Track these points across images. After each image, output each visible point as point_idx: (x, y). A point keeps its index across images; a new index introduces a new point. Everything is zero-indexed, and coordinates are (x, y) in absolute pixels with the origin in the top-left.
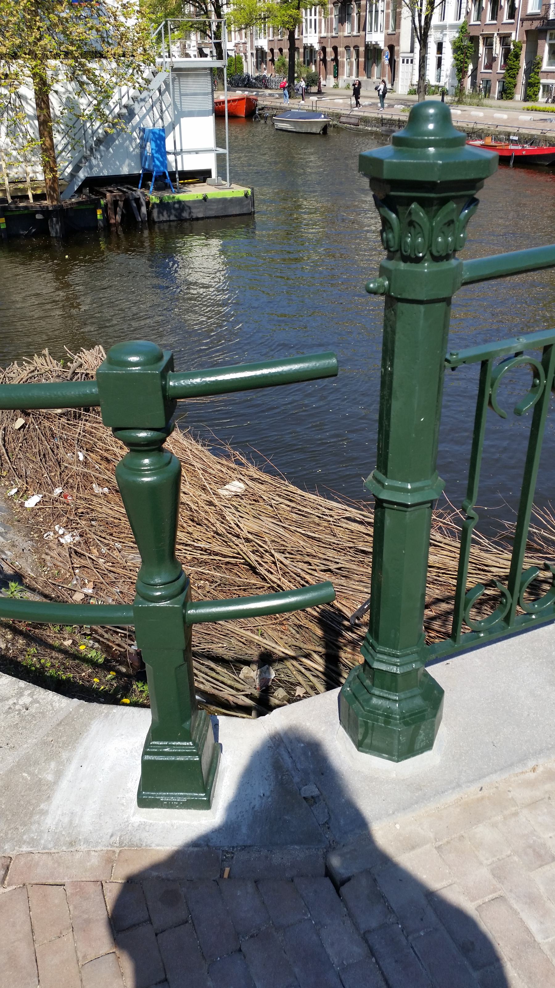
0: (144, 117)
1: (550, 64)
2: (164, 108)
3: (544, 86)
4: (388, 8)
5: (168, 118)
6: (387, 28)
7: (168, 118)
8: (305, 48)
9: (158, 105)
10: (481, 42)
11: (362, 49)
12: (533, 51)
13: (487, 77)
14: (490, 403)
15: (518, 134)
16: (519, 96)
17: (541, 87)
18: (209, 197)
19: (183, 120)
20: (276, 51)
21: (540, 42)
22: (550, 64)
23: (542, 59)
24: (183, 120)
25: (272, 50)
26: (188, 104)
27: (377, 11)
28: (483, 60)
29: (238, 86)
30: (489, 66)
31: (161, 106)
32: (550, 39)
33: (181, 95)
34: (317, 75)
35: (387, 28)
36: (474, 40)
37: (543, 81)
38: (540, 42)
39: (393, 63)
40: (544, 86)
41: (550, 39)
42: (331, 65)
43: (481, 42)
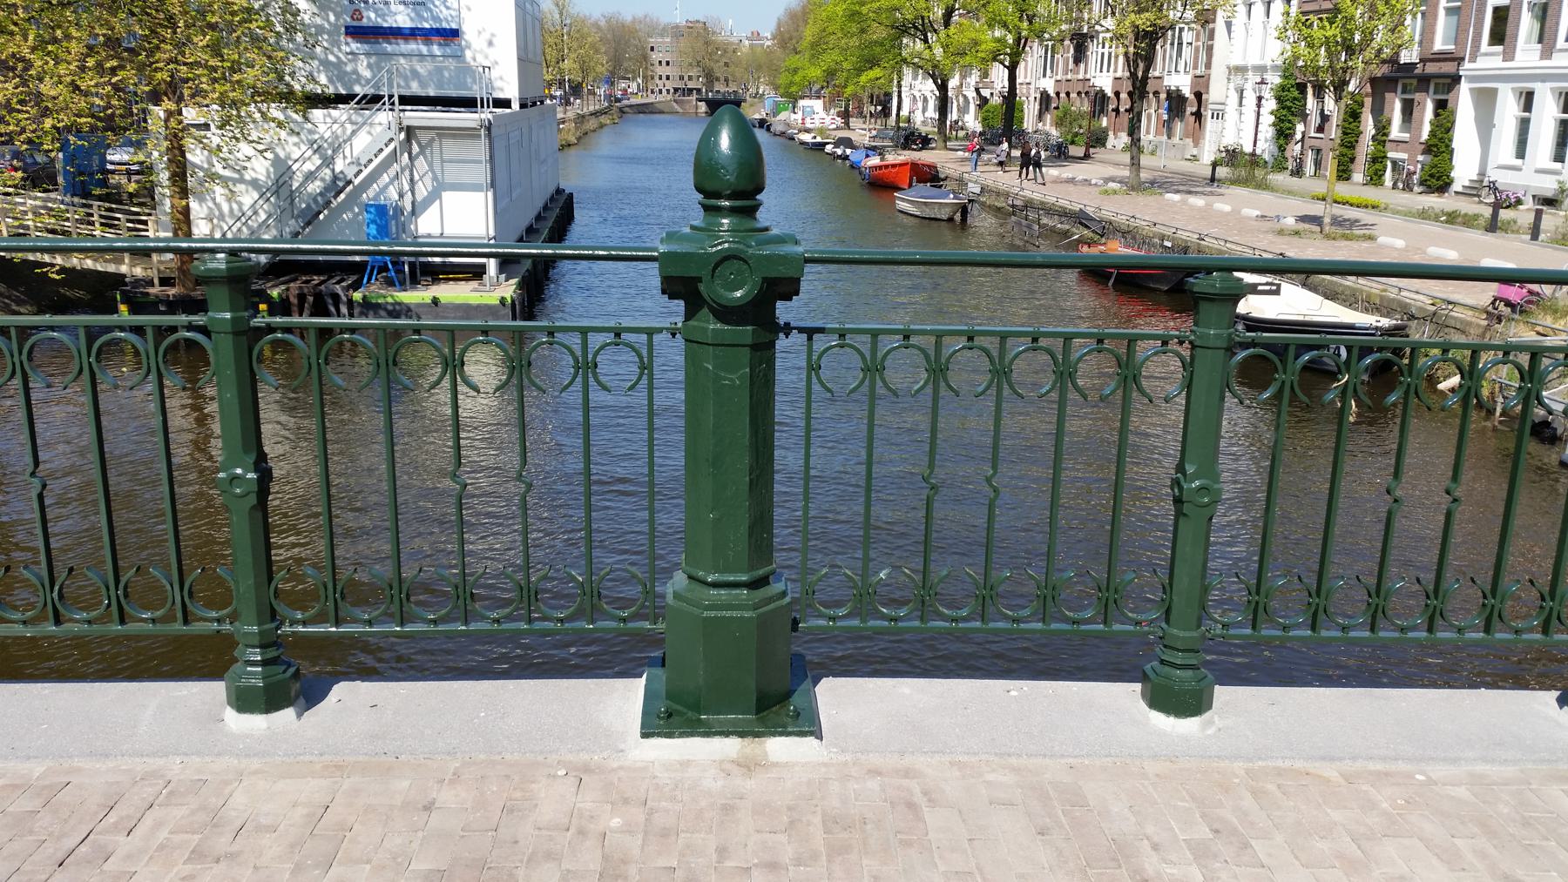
0: (386, 186)
1: (1402, 131)
2: (416, 177)
3: (1394, 163)
4: (1198, 40)
5: (422, 191)
6: (1195, 67)
7: (422, 191)
8: (1169, 93)
9: (407, 173)
10: (1310, 91)
11: (1163, 96)
12: (1378, 110)
13: (1317, 143)
14: (1559, 618)
15: (1173, 240)
16: (1358, 177)
17: (1389, 164)
18: (443, 301)
19: (445, 195)
20: (1063, 95)
21: (1388, 95)
22: (1402, 131)
23: (1389, 122)
24: (445, 195)
25: (1058, 94)
26: (452, 173)
27: (1180, 44)
28: (1314, 120)
29: (1345, 133)
30: (1320, 129)
31: (412, 175)
32: (1404, 92)
33: (443, 161)
34: (1105, 132)
35: (1195, 67)
36: (1302, 88)
37: (1390, 155)
38: (1388, 95)
39: (1198, 115)
40: (1394, 163)
41: (1404, 92)
42: (1125, 118)
43: (1310, 91)
